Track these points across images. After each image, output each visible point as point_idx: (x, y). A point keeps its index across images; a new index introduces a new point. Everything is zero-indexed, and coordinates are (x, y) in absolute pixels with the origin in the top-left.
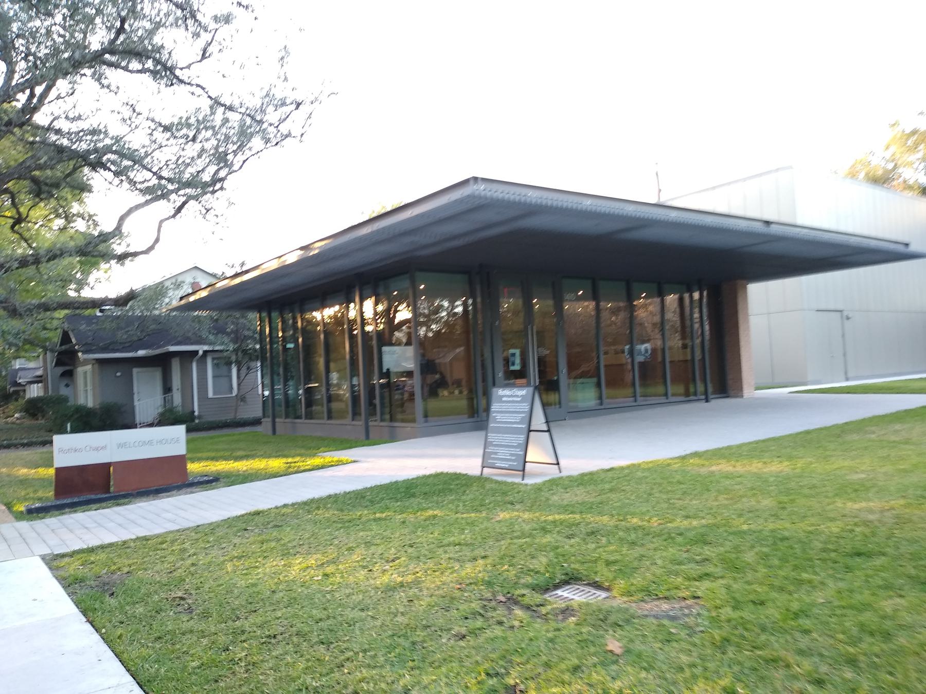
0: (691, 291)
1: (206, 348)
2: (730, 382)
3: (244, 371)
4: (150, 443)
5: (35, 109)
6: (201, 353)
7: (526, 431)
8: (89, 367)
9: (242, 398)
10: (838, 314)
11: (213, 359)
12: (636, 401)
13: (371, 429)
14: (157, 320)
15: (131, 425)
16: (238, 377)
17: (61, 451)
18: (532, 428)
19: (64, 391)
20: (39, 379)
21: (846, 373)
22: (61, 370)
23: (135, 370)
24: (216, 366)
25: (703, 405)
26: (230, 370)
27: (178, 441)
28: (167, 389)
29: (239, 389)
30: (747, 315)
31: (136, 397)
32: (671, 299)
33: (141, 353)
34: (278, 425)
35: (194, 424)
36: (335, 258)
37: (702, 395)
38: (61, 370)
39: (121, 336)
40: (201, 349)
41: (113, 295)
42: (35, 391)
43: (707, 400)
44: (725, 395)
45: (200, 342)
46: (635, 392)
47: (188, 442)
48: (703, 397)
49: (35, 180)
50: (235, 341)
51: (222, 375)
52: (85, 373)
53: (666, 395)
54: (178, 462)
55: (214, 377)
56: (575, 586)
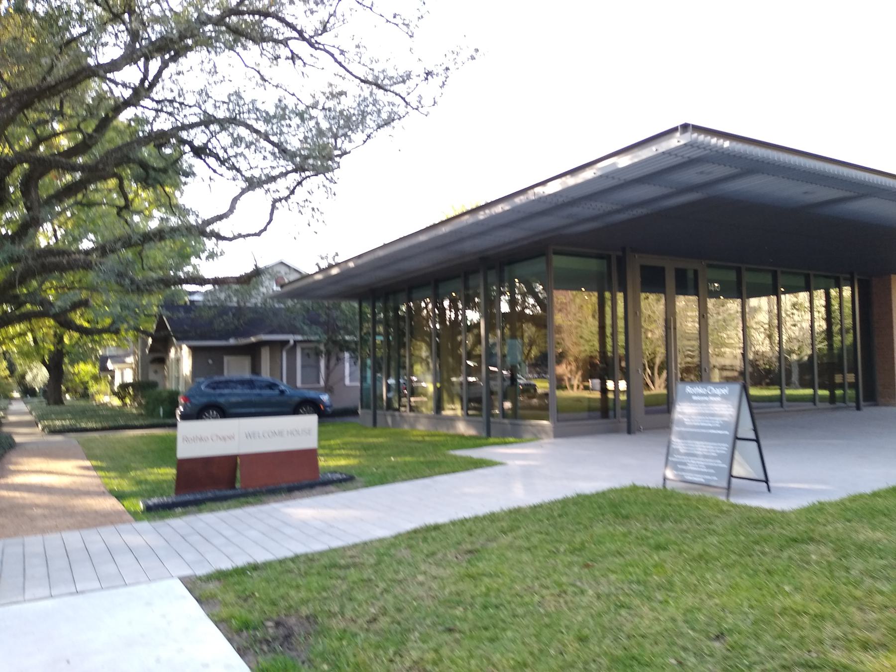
0: (839, 286)
1: (299, 338)
3: (333, 362)
4: (281, 433)
6: (292, 342)
7: (731, 439)
11: (303, 349)
12: (782, 406)
13: (492, 426)
14: (255, 310)
17: (186, 439)
18: (739, 436)
19: (152, 377)
23: (226, 359)
24: (306, 355)
26: (318, 362)
27: (309, 432)
32: (819, 295)
33: (232, 342)
34: (378, 417)
35: (325, 415)
36: (404, 259)
39: (219, 324)
40: (291, 338)
41: (237, 273)
43: (858, 408)
45: (293, 332)
47: (320, 433)
48: (854, 404)
50: (326, 332)
51: (311, 368)
54: (308, 456)
55: (303, 367)
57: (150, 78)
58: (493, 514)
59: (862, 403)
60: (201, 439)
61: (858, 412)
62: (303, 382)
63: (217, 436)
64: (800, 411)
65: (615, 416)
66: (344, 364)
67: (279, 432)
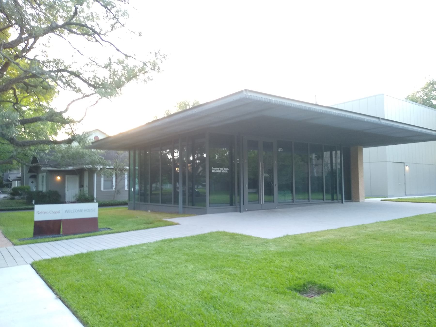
2: (353, 194)
4: (81, 211)
5: (28, 51)
8: (44, 174)
9: (118, 192)
10: (403, 164)
12: (309, 201)
15: (64, 202)
16: (116, 182)
17: (38, 213)
20: (19, 179)
21: (405, 193)
22: (30, 174)
25: (340, 204)
28: (81, 186)
29: (116, 187)
30: (362, 163)
31: (66, 189)
33: (70, 168)
37: (340, 200)
38: (30, 174)
42: (16, 184)
44: (350, 200)
46: (324, 197)
48: (341, 201)
49: (25, 84)
52: (43, 176)
53: (323, 199)
55: (104, 181)
56: (310, 295)
57: (29, 45)
58: (171, 239)
59: (344, 200)
60: (45, 213)
61: (342, 204)
62: (104, 189)
63: (52, 211)
64: (319, 203)
65: (235, 205)
66: (125, 180)
67: (80, 210)
